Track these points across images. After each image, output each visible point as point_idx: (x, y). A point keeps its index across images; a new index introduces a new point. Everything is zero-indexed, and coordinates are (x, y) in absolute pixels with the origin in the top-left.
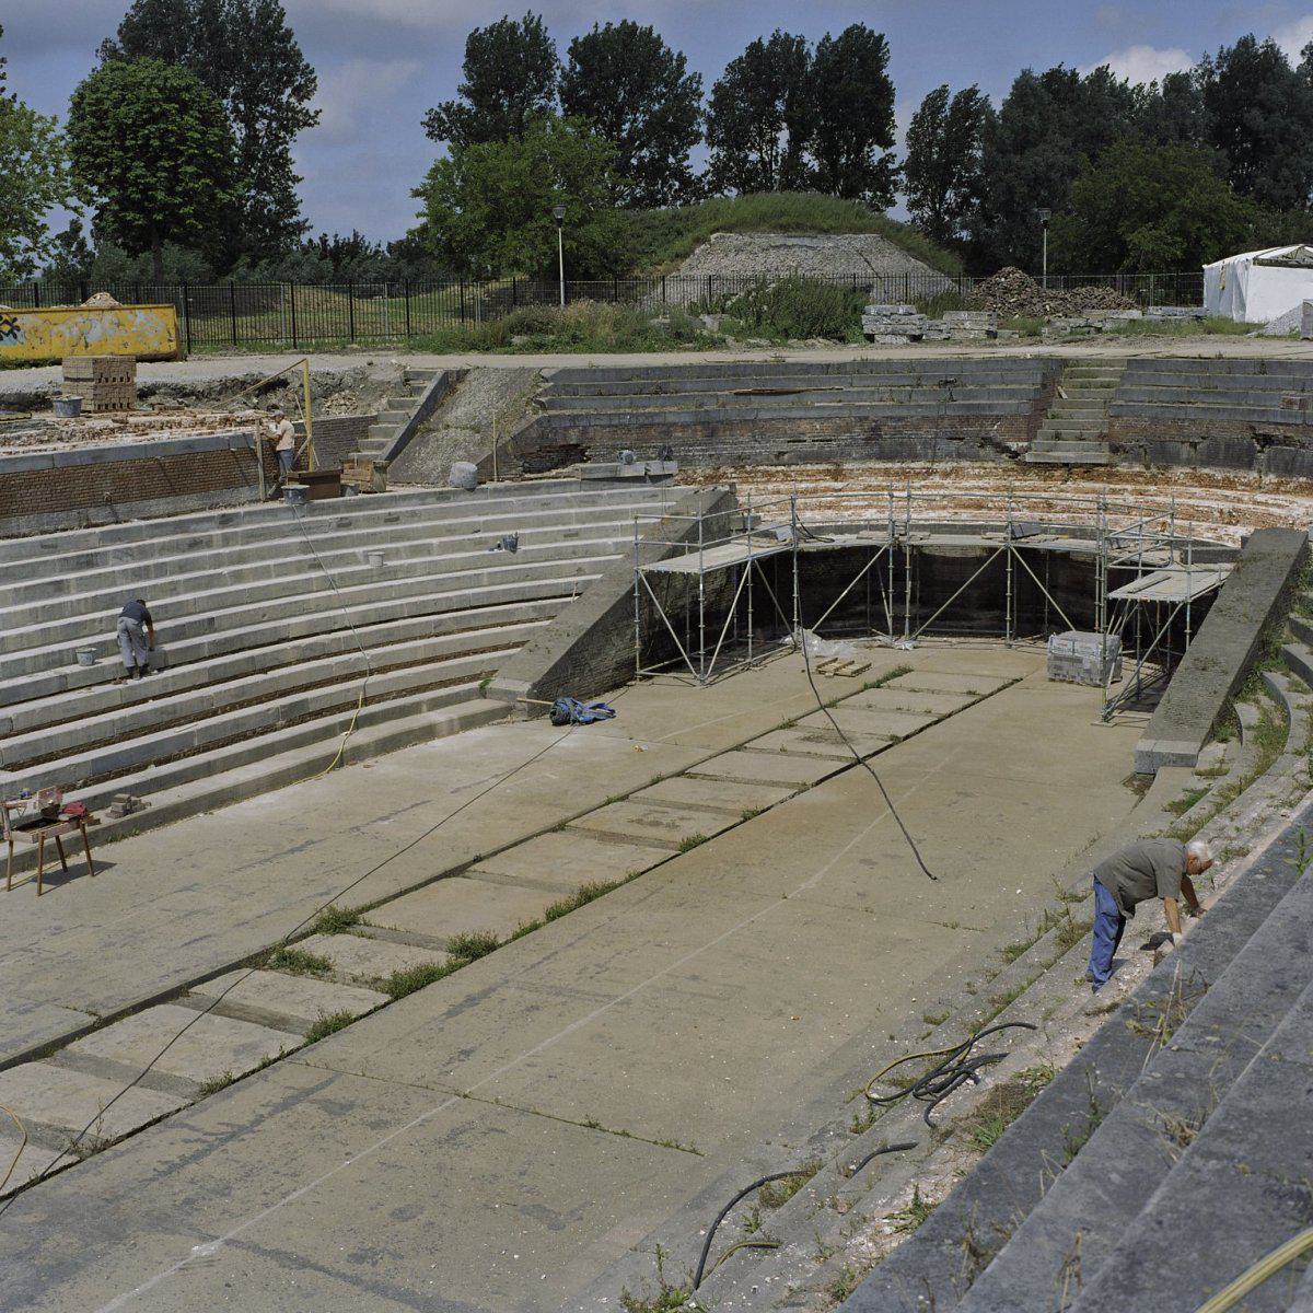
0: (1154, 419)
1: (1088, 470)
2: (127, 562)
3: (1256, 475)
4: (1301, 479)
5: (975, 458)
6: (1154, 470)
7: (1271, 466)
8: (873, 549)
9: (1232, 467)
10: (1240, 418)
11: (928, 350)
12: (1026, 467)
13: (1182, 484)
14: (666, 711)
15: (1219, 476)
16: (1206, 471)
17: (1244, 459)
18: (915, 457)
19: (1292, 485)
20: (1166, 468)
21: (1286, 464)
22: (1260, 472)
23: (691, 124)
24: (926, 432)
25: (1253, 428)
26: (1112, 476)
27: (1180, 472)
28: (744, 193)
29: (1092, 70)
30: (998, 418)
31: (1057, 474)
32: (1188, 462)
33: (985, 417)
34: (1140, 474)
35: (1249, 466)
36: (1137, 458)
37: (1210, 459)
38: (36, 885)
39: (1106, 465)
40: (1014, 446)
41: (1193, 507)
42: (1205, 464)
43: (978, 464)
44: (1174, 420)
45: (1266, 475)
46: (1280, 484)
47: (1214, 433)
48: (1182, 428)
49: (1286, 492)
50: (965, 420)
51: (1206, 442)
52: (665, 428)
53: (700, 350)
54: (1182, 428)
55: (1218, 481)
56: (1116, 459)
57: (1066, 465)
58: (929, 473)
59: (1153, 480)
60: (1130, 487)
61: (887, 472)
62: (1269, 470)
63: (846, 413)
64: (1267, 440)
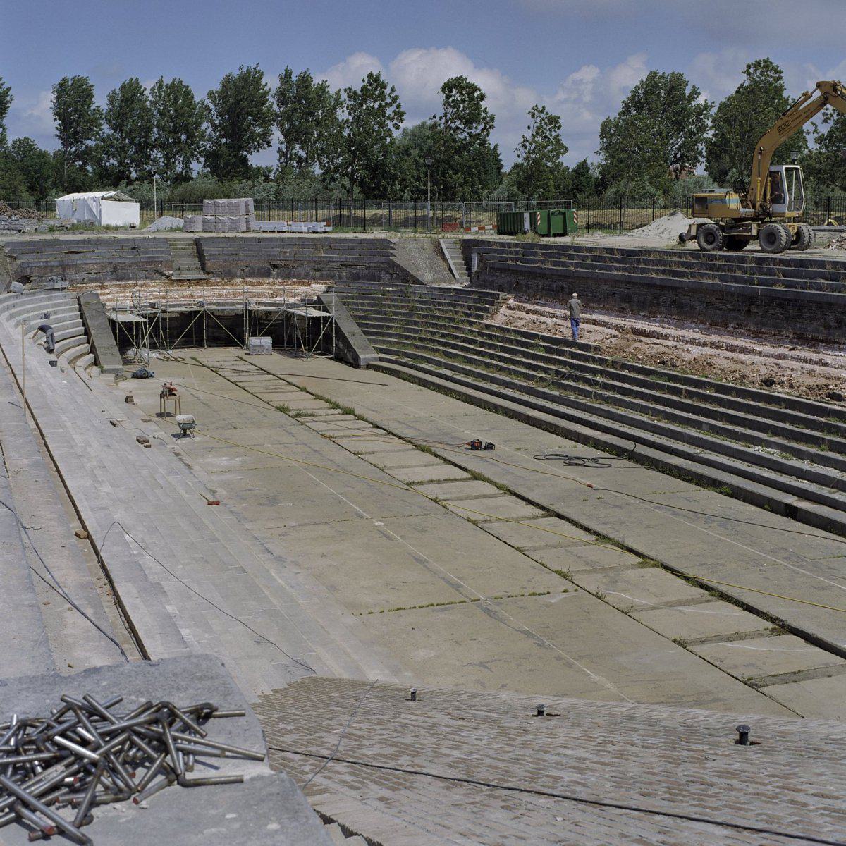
5: (152, 279)
15: (255, 281)
18: (130, 279)
20: (231, 279)
24: (133, 268)
26: (208, 284)
27: (237, 280)
30: (161, 262)
32: (241, 276)
34: (220, 282)
35: (269, 276)
36: (218, 276)
37: (251, 275)
50: (149, 263)
56: (208, 277)
62: (278, 277)
64: (275, 267)
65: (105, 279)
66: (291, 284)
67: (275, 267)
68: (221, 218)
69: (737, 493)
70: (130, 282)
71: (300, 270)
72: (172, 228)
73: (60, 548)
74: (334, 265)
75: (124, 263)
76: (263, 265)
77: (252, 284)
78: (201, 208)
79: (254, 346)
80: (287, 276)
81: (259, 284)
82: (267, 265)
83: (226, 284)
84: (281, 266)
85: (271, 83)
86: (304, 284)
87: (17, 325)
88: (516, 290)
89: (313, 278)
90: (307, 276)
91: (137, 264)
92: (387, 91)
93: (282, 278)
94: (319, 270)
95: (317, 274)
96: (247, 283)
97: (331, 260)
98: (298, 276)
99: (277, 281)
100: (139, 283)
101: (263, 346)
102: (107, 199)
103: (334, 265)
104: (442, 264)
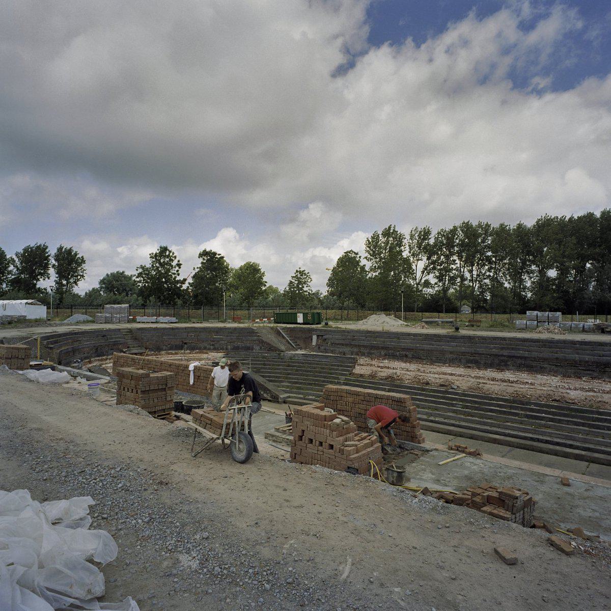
2: (570, 425)
9: (177, 350)
15: (173, 352)
17: (181, 348)
18: (104, 356)
23: (381, 278)
24: (107, 349)
28: (83, 276)
29: (56, 251)
30: (121, 344)
32: (165, 350)
35: (182, 349)
36: (153, 350)
37: (171, 349)
40: (124, 350)
47: (172, 343)
50: (114, 345)
53: (25, 328)
58: (107, 359)
61: (99, 360)
63: (91, 345)
64: (186, 343)
65: (92, 357)
66: (195, 353)
67: (186, 343)
69: (556, 454)
71: (202, 345)
72: (84, 321)
75: (102, 346)
76: (178, 343)
77: (172, 354)
81: (176, 354)
82: (181, 343)
83: (157, 355)
85: (52, 251)
86: (203, 353)
87: (385, 419)
88: (370, 355)
89: (209, 349)
90: (205, 348)
91: (108, 346)
92: (174, 263)
93: (189, 350)
94: (213, 345)
95: (212, 347)
96: (169, 354)
98: (200, 349)
100: (109, 357)
102: (29, 304)
104: (284, 341)
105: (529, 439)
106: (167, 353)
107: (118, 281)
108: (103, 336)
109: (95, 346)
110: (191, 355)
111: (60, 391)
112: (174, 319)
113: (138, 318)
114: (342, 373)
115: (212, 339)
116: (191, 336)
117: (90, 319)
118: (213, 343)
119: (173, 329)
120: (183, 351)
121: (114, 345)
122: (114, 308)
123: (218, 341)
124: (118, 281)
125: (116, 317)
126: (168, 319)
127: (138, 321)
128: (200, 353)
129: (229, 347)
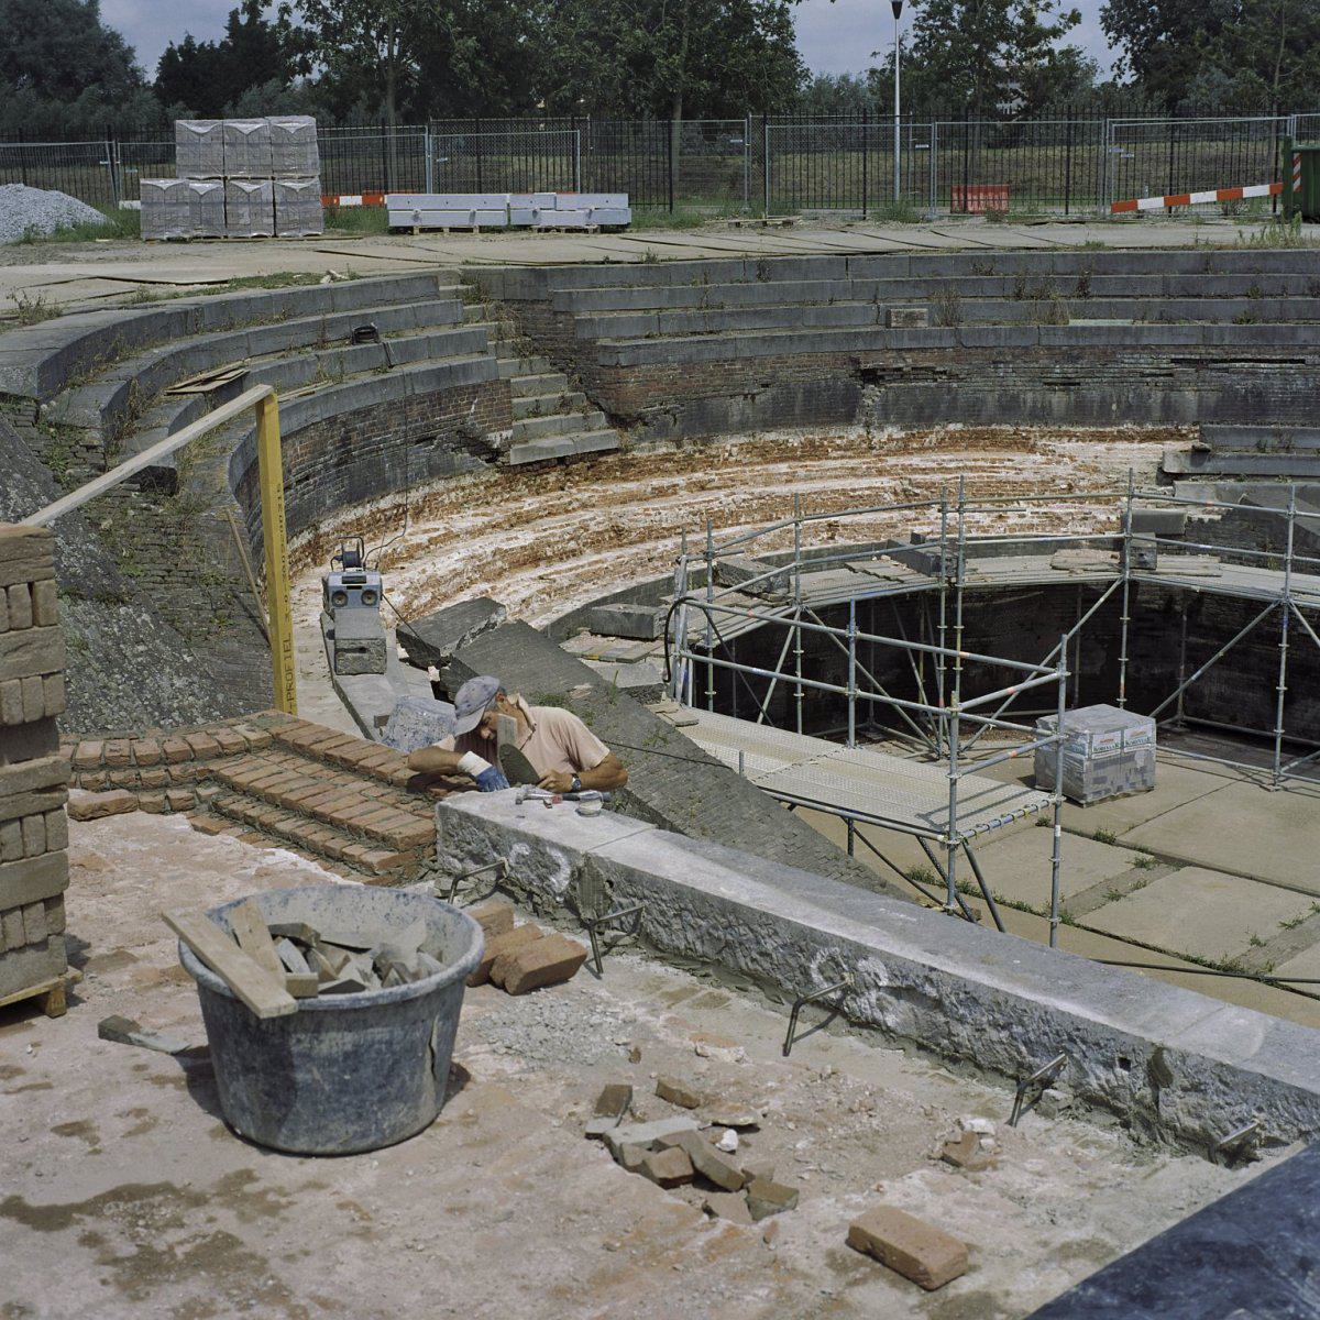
0: (687, 365)
1: (590, 464)
3: (862, 431)
4: (951, 427)
5: (449, 472)
6: (689, 448)
7: (887, 414)
8: (1086, 592)
9: (817, 424)
10: (832, 348)
11: (55, 272)
12: (514, 473)
13: (738, 463)
14: (365, 947)
15: (795, 441)
16: (772, 436)
17: (843, 409)
18: (383, 488)
19: (933, 438)
20: (706, 442)
21: (921, 408)
22: (867, 425)
25: (856, 362)
26: (628, 469)
27: (730, 444)
30: (475, 390)
31: (552, 478)
32: (743, 427)
33: (460, 391)
34: (667, 458)
35: (849, 419)
36: (662, 432)
37: (779, 416)
38: (690, 1171)
39: (616, 450)
41: (844, 492)
42: (768, 425)
43: (453, 484)
44: (718, 362)
45: (881, 428)
46: (907, 441)
48: (731, 373)
49: (922, 449)
51: (770, 392)
52: (1208, 467)
54: (731, 373)
55: (794, 449)
56: (629, 437)
57: (561, 461)
59: (688, 464)
60: (680, 480)
62: (886, 419)
64: (871, 376)
67: (871, 376)
68: (248, 187)
70: (385, 503)
72: (58, 230)
73: (99, 1285)
74: (1145, 363)
77: (786, 454)
78: (168, 156)
79: (1099, 765)
80: (919, 416)
81: (813, 451)
82: (844, 374)
84: (900, 374)
86: (995, 441)
89: (1041, 415)
90: (1010, 408)
91: (400, 408)
93: (902, 420)
94: (1067, 384)
95: (1058, 399)
96: (765, 454)
97: (1130, 343)
98: (972, 412)
99: (880, 437)
101: (1130, 757)
103: (1145, 363)
105: (1030, 547)
106: (751, 449)
107: (33, 36)
108: (358, 337)
109: (332, 421)
110: (916, 461)
111: (531, 1138)
112: (616, 205)
113: (401, 206)
114: (186, 332)
115: (1060, 340)
116: (911, 318)
117: (90, 214)
118: (1069, 368)
119: (764, 268)
120: (855, 433)
121: (437, 400)
122: (236, 140)
123: (1107, 356)
124: (33, 36)
125: (250, 200)
126: (576, 207)
127: (396, 220)
128: (974, 440)
129: (1190, 396)
